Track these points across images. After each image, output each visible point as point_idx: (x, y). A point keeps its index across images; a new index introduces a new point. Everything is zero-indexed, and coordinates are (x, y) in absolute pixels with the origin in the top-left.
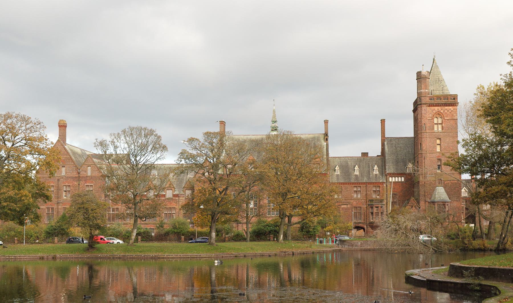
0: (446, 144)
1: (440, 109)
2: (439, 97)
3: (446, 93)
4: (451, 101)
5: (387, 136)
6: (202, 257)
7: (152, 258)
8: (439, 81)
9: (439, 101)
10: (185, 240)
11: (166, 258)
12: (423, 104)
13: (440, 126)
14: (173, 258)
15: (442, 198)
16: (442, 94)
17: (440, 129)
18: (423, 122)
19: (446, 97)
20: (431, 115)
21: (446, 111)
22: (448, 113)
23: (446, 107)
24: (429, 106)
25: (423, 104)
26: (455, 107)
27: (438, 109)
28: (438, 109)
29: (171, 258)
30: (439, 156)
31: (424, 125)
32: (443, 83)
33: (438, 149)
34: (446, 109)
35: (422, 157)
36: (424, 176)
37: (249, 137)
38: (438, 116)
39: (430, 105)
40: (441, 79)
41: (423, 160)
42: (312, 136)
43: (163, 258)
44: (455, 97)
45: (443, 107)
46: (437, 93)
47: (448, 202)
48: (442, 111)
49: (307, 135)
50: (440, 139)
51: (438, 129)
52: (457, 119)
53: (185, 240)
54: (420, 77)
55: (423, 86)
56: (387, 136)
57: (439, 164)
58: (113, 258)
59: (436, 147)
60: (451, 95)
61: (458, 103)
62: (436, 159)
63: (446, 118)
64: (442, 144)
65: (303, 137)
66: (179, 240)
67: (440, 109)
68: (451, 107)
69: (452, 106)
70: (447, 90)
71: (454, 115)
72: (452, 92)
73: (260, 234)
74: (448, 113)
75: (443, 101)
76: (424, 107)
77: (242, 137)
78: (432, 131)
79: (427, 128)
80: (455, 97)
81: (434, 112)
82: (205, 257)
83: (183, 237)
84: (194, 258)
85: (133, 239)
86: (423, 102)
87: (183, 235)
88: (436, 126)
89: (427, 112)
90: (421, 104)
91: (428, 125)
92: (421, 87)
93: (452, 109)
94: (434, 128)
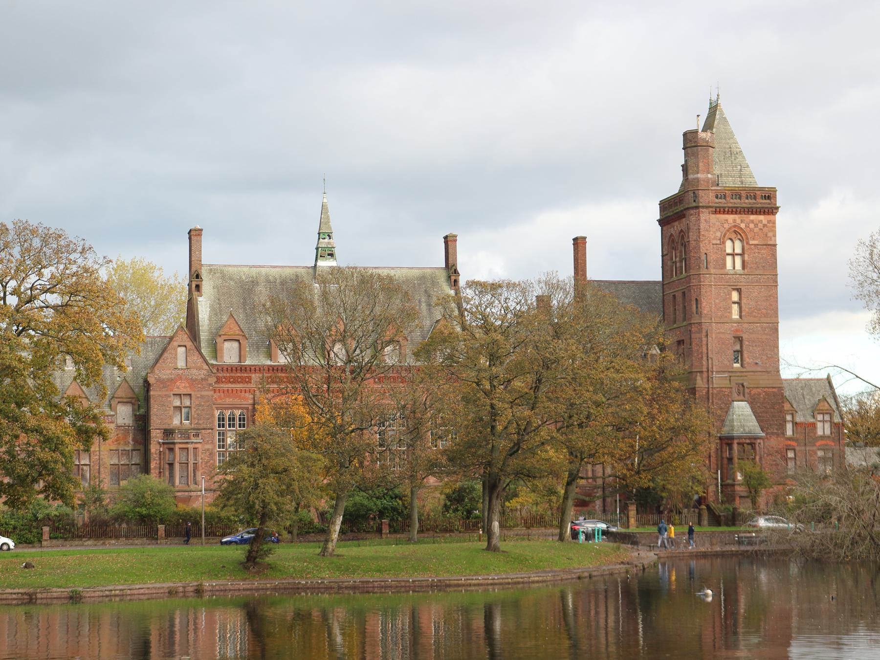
0: (753, 303)
1: (738, 221)
2: (736, 194)
3: (748, 182)
4: (762, 202)
5: (593, 273)
6: (533, 582)
7: (432, 586)
8: (733, 154)
9: (736, 202)
10: (168, 535)
11: (463, 585)
12: (703, 207)
13: (738, 260)
14: (479, 585)
15: (747, 429)
16: (738, 185)
17: (738, 266)
18: (703, 250)
19: (753, 193)
20: (718, 234)
21: (752, 226)
22: (756, 230)
23: (752, 217)
24: (716, 212)
25: (703, 207)
26: (770, 217)
27: (734, 221)
28: (734, 221)
29: (475, 585)
30: (737, 331)
31: (703, 257)
32: (740, 158)
33: (735, 316)
34: (752, 221)
35: (700, 331)
36: (705, 375)
37: (263, 271)
38: (733, 236)
39: (719, 210)
40: (734, 150)
41: (704, 339)
42: (416, 273)
43: (458, 585)
44: (769, 195)
45: (744, 216)
46: (730, 182)
47: (760, 438)
48: (743, 226)
49: (405, 271)
50: (739, 291)
51: (732, 265)
52: (775, 245)
53: (168, 535)
54: (691, 141)
55: (701, 164)
56: (593, 273)
57: (738, 348)
58: (340, 588)
59: (730, 308)
60: (761, 189)
61: (777, 208)
62: (730, 336)
63: (751, 242)
64: (744, 301)
65: (397, 274)
66: (152, 536)
67: (738, 221)
68: (761, 217)
69: (764, 213)
70: (751, 176)
71: (770, 234)
72: (762, 181)
73: (358, 516)
74: (756, 230)
75: (746, 203)
76: (705, 215)
77: (246, 270)
78: (721, 272)
79: (711, 265)
80: (769, 195)
81: (726, 226)
82: (537, 582)
83: (161, 527)
84: (518, 583)
85: (335, 540)
86: (703, 202)
87: (162, 522)
88: (729, 259)
89: (710, 227)
90: (697, 207)
91: (712, 257)
92: (698, 167)
93: (765, 222)
94: (725, 264)
